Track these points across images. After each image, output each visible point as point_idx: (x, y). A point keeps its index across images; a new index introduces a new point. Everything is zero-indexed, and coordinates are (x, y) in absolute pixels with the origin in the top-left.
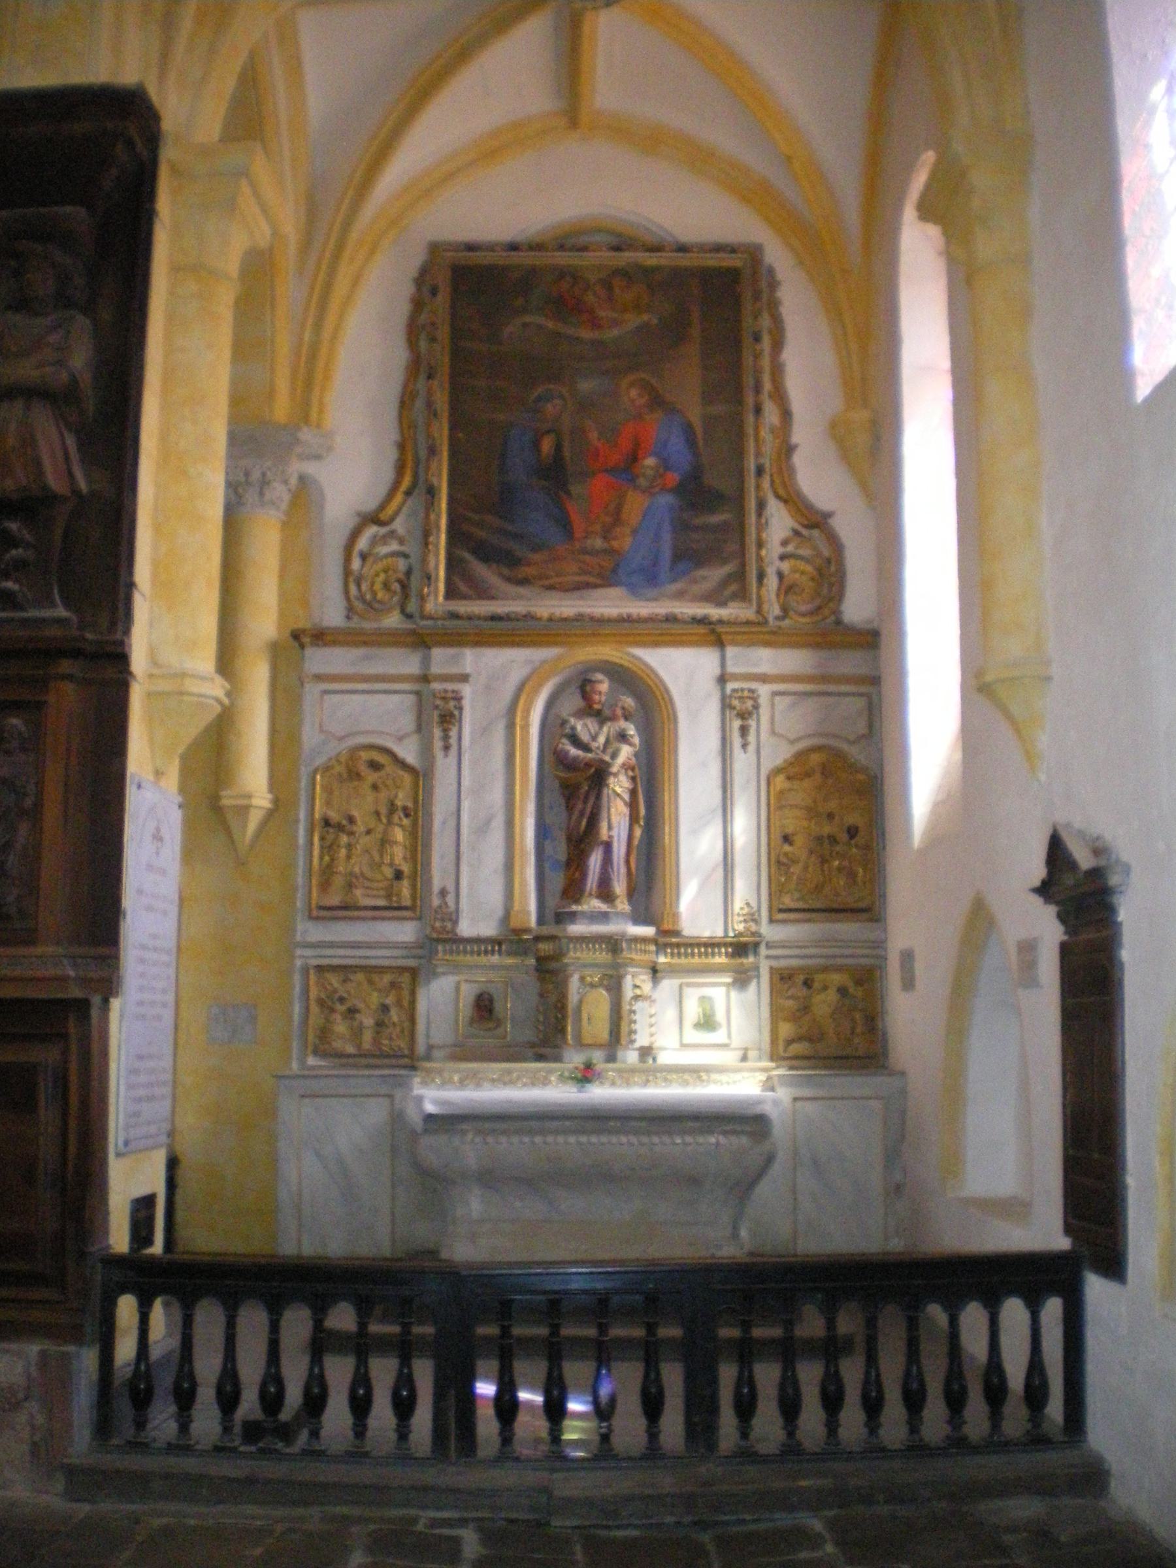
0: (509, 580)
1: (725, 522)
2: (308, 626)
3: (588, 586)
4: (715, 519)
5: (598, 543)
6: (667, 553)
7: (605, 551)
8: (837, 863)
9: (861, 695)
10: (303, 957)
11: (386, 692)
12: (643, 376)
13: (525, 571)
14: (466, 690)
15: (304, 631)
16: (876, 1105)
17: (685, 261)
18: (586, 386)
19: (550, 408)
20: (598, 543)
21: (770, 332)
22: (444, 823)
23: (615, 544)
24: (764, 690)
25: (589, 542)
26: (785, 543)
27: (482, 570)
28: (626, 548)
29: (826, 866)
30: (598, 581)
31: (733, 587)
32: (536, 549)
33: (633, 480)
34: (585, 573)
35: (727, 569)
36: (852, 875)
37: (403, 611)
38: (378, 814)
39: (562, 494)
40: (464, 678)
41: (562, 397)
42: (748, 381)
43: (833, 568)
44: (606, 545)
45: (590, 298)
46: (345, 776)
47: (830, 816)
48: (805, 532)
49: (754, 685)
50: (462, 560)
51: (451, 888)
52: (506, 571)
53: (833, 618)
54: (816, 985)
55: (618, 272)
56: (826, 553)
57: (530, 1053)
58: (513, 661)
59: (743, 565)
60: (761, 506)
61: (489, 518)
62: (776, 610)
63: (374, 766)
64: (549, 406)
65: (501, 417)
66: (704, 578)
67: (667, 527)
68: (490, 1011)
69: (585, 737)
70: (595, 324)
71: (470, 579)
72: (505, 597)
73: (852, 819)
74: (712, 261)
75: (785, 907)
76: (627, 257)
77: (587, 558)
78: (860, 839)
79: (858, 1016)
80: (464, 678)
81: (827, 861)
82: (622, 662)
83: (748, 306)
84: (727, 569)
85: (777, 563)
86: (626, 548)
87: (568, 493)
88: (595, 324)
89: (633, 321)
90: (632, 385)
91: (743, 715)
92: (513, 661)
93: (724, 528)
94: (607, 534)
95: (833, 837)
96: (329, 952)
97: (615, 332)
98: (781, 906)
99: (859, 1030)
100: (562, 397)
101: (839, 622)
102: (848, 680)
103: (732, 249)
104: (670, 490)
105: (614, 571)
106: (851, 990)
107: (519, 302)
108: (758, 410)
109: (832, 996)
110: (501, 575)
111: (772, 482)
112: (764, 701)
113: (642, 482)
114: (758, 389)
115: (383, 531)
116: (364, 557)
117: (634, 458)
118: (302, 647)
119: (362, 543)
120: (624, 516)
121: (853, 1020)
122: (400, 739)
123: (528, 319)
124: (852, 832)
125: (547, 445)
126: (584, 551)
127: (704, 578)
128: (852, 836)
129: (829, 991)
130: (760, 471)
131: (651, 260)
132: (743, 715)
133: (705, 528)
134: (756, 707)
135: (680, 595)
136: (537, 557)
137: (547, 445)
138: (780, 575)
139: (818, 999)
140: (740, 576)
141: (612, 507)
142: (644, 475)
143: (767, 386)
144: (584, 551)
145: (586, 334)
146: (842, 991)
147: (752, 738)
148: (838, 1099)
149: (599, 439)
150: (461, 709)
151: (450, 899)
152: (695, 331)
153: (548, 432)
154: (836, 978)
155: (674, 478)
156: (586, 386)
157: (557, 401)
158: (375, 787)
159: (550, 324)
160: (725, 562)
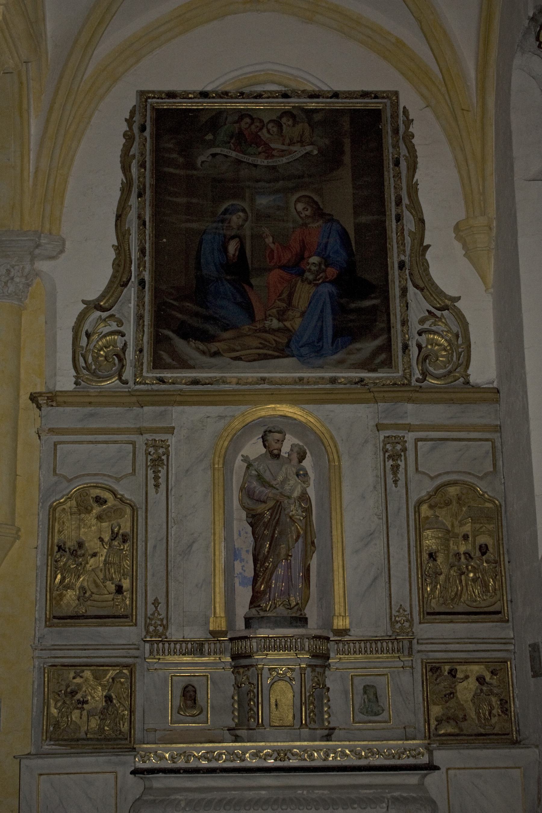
0: (204, 353)
1: (374, 305)
2: (44, 390)
3: (266, 357)
4: (367, 303)
5: (275, 324)
6: (329, 332)
7: (279, 330)
8: (471, 575)
9: (487, 440)
10: (41, 657)
11: (106, 442)
12: (307, 193)
13: (214, 347)
14: (172, 441)
15: (41, 394)
16: (517, 773)
17: (339, 104)
18: (263, 201)
19: (235, 219)
20: (275, 324)
21: (406, 159)
22: (155, 547)
23: (288, 324)
24: (410, 437)
25: (267, 323)
26: (422, 321)
27: (180, 344)
28: (296, 327)
29: (463, 577)
30: (276, 354)
31: (383, 356)
32: (225, 329)
33: (301, 273)
34: (264, 347)
35: (378, 342)
36: (485, 585)
37: (120, 379)
38: (101, 540)
39: (247, 287)
40: (171, 430)
41: (244, 210)
42: (391, 196)
43: (460, 341)
44: (281, 325)
45: (264, 135)
46: (74, 510)
47: (466, 537)
48: (438, 313)
49: (401, 433)
50: (168, 339)
51: (162, 600)
52: (202, 346)
53: (462, 380)
54: (460, 675)
55: (286, 113)
56: (455, 329)
57: (325, 739)
58: (208, 417)
59: (389, 340)
60: (404, 291)
61: (188, 304)
62: (418, 375)
63: (100, 501)
64: (234, 218)
65: (195, 225)
66: (359, 350)
67: (328, 310)
68: (194, 701)
69: (267, 476)
70: (269, 153)
71: (174, 354)
72: (202, 368)
73: (482, 539)
74: (359, 104)
75: (432, 611)
76: (294, 101)
77: (265, 335)
78: (490, 555)
79: (494, 700)
80: (171, 430)
81: (463, 573)
82: (295, 416)
83: (388, 139)
84: (378, 342)
85: (417, 337)
86: (296, 327)
87: (251, 286)
88: (269, 153)
89: (299, 151)
90: (298, 200)
91: (395, 457)
92: (208, 417)
93: (374, 308)
94: (281, 316)
95: (467, 553)
96: (59, 653)
97: (284, 160)
98: (429, 611)
99: (494, 712)
100: (244, 210)
101: (467, 383)
102: (474, 428)
103: (376, 95)
104: (330, 282)
105: (288, 345)
106: (488, 679)
107: (209, 137)
108: (399, 218)
109: (472, 684)
110: (198, 349)
111: (411, 274)
112: (410, 446)
113: (308, 275)
114: (399, 202)
115: (105, 315)
116: (88, 335)
117: (301, 257)
118: (39, 407)
119: (87, 326)
120: (295, 302)
121: (490, 705)
122: (118, 480)
123: (217, 150)
124: (484, 550)
125: (232, 247)
126: (264, 330)
127: (359, 350)
128: (483, 554)
129: (470, 680)
130: (402, 265)
131: (312, 104)
132: (395, 457)
133: (359, 311)
134: (404, 450)
135: (340, 363)
136: (227, 335)
137: (232, 247)
138: (420, 347)
139: (460, 687)
140: (387, 347)
141: (284, 296)
142: (310, 270)
143: (406, 201)
144: (264, 330)
145: (261, 161)
146: (481, 680)
147: (401, 475)
148: (493, 768)
149: (274, 243)
150: (167, 454)
151: (162, 608)
152: (347, 159)
153: (233, 237)
154: (476, 670)
155: (332, 272)
156: (263, 201)
157: (241, 214)
158: (99, 518)
159: (234, 154)
160: (375, 337)
